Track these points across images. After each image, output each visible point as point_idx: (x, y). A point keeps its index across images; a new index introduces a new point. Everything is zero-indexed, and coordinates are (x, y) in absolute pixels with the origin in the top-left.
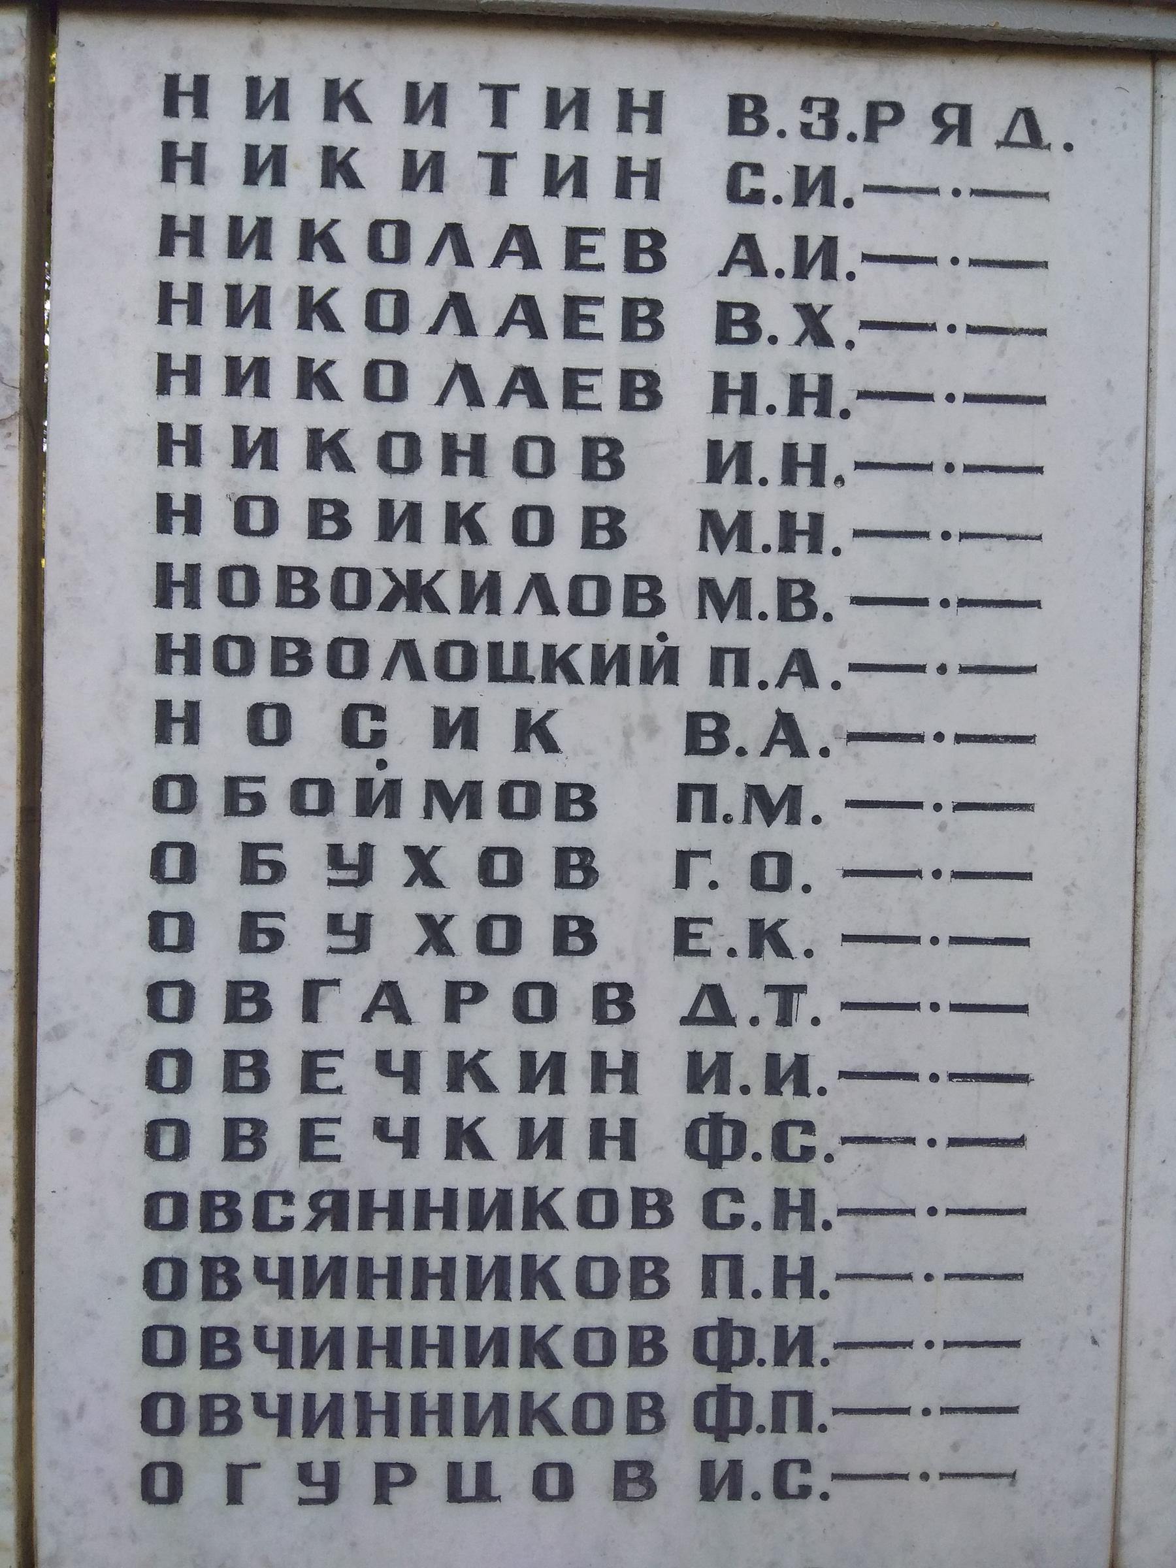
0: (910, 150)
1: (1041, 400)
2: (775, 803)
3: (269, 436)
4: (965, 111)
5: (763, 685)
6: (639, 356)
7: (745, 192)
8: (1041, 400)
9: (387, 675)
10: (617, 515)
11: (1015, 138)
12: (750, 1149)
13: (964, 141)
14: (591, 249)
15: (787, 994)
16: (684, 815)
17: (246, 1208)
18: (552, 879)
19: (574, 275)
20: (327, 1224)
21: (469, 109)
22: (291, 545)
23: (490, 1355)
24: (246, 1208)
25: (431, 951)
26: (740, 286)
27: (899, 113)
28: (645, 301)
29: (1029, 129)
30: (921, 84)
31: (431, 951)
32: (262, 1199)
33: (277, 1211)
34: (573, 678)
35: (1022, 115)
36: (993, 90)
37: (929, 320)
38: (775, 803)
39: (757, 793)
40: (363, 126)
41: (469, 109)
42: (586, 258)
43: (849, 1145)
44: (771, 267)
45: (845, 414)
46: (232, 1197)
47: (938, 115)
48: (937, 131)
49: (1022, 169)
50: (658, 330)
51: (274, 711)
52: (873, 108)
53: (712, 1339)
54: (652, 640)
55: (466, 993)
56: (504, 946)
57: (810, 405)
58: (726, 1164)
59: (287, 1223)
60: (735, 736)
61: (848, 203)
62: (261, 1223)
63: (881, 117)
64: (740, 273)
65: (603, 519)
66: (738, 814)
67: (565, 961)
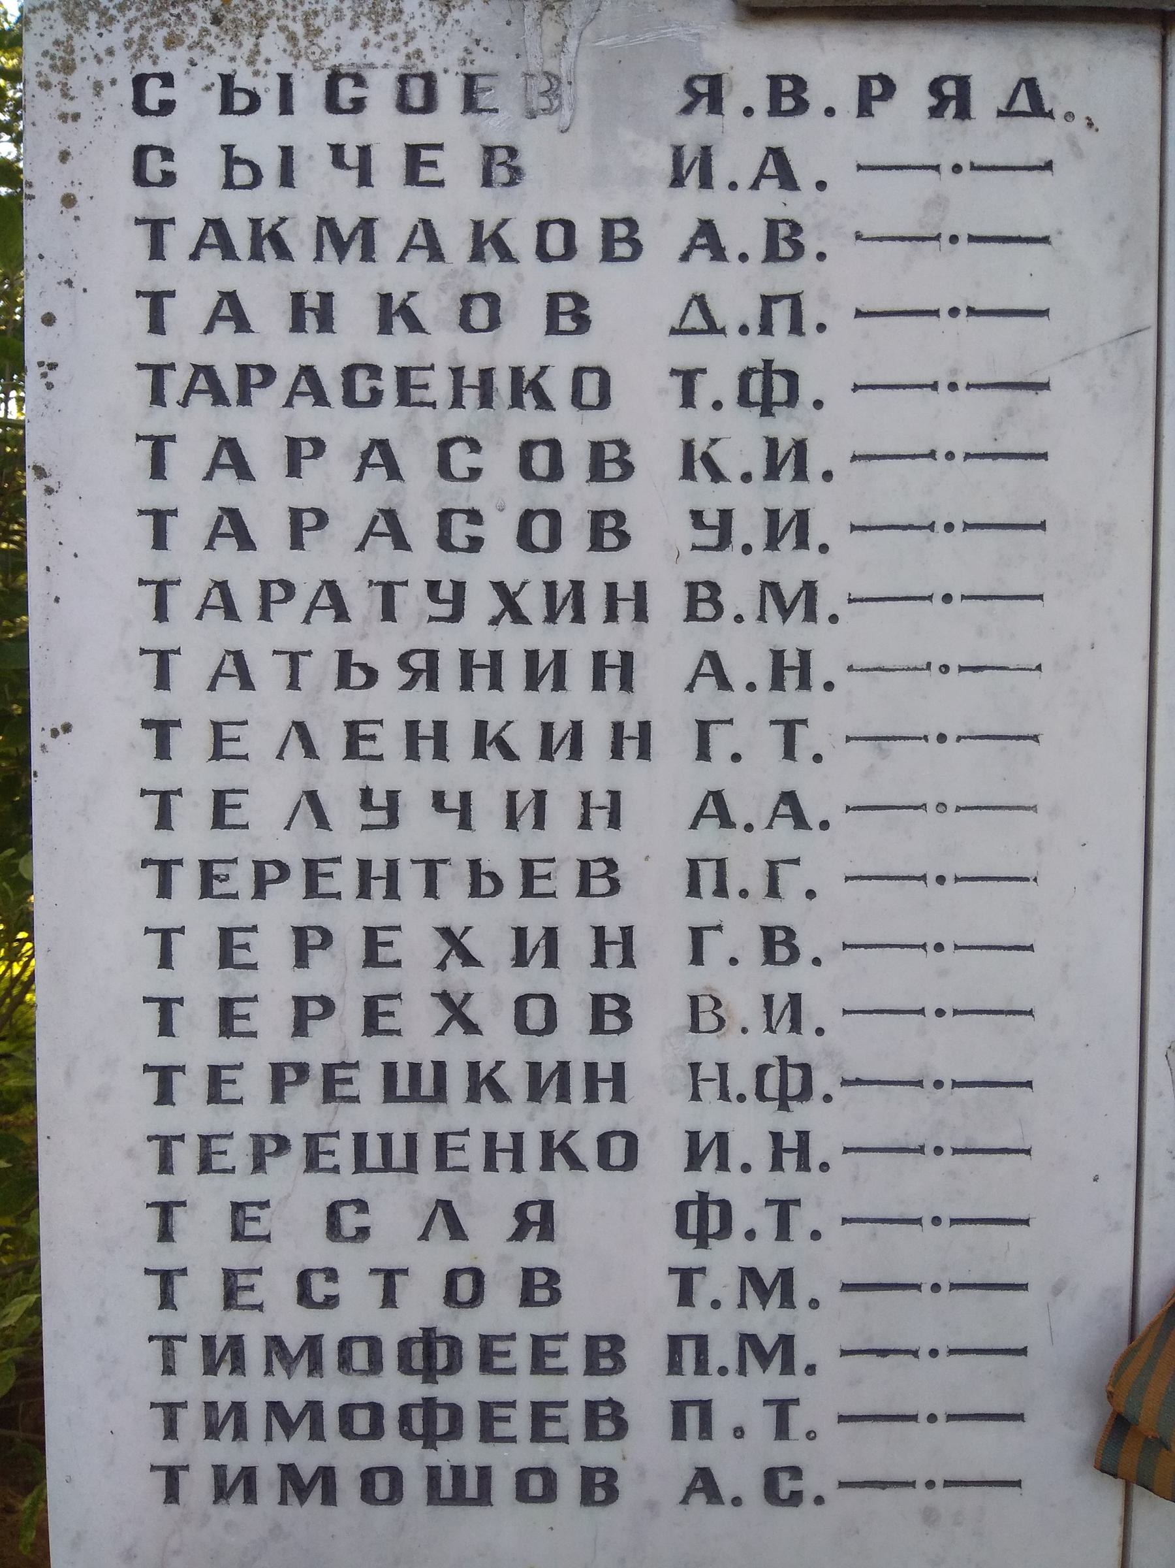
0: (906, 119)
1: (1044, 456)
2: (768, 1351)
3: (213, 1431)
4: (963, 83)
5: (716, 1304)
6: (608, 496)
8: (1044, 456)
11: (1017, 107)
12: (739, 1226)
13: (963, 113)
14: (556, 1354)
15: (784, 1208)
16: (679, 1432)
22: (273, 555)
26: (709, 840)
27: (889, 87)
28: (615, 996)
29: (1030, 101)
30: (916, 55)
35: (1023, 86)
36: (990, 59)
37: (910, 1411)
38: (768, 1351)
39: (748, 1341)
40: (285, 263)
42: (551, 1363)
45: (834, 619)
47: (935, 87)
48: (934, 102)
50: (627, 1023)
52: (865, 81)
53: (714, 1225)
56: (476, 1496)
57: (792, 678)
58: (712, 1242)
60: (721, 171)
61: (824, 1167)
63: (874, 91)
64: (709, 826)
65: (566, 304)
66: (733, 1364)
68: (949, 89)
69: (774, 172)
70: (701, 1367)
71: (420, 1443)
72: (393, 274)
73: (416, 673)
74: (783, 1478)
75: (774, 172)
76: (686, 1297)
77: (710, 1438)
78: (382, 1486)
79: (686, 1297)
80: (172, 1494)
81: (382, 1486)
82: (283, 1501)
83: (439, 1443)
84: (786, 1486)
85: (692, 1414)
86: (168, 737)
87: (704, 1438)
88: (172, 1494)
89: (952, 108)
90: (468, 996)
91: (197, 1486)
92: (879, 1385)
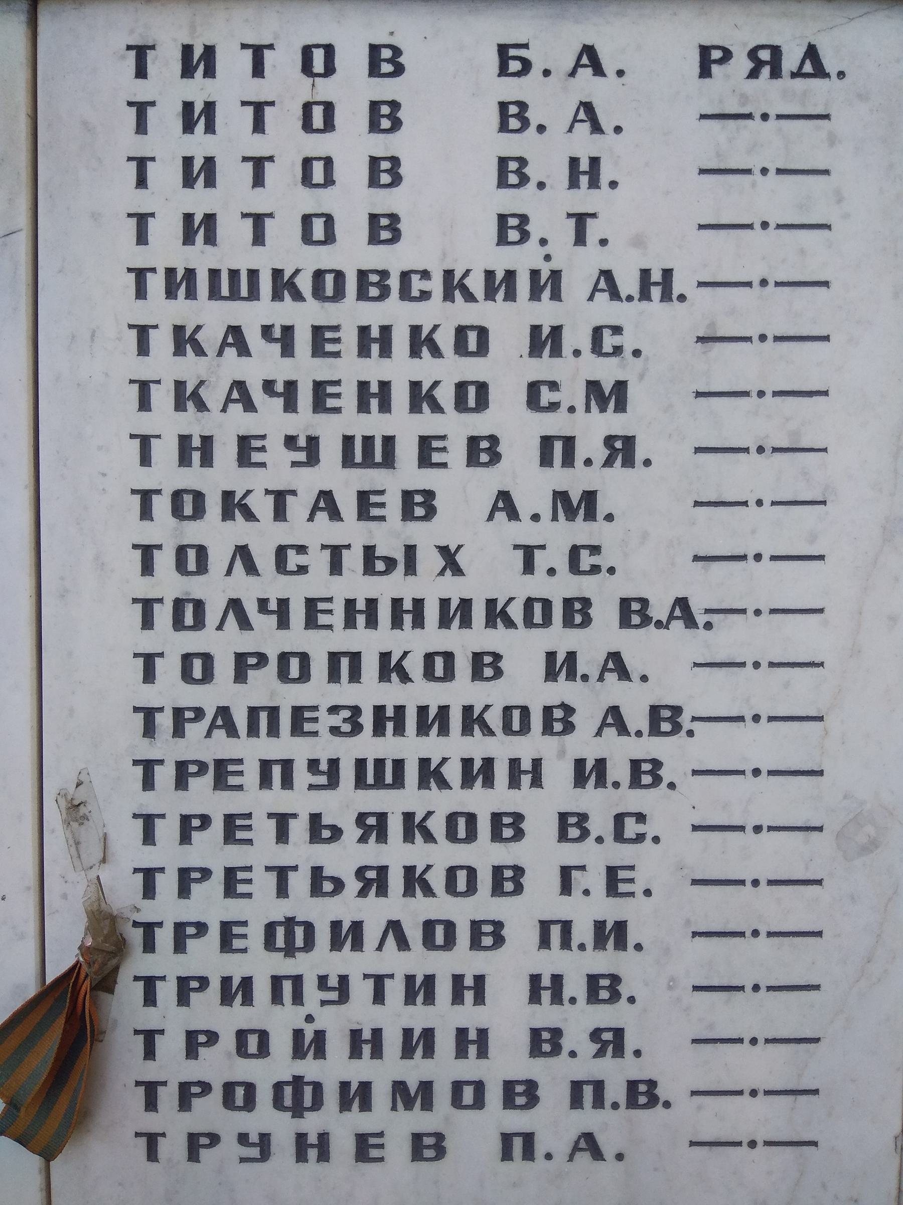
4: (776, 51)
7: (415, 293)
9: (220, 627)
10: (519, 871)
11: (578, 118)
17: (394, 283)
18: (496, 70)
19: (233, 848)
20: (619, 461)
21: (233, 63)
23: (582, 512)
24: (394, 283)
25: (448, 572)
29: (814, 63)
31: (448, 572)
32: (405, 276)
33: (417, 285)
34: (510, 623)
41: (233, 63)
43: (742, 554)
44: (632, 729)
46: (384, 274)
47: (753, 54)
49: (817, 93)
51: (322, 107)
54: (539, 263)
55: (196, 823)
59: (425, 295)
62: (405, 294)
67: (540, 1062)
68: (765, 55)
69: (605, 288)
70: (566, 943)
71: (290, 1114)
72: (584, 743)
73: (605, 1044)
74: (584, 554)
75: (605, 288)
76: (529, 567)
77: (251, 1004)
78: (468, 1094)
79: (529, 567)
80: (152, 1154)
81: (468, 1094)
82: (394, 1108)
83: (306, 1114)
84: (546, 396)
85: (287, 986)
86: (263, 58)
87: (182, 1005)
88: (152, 1154)
89: (766, 71)
90: (459, 547)
91: (173, 1147)
92: (718, 907)
